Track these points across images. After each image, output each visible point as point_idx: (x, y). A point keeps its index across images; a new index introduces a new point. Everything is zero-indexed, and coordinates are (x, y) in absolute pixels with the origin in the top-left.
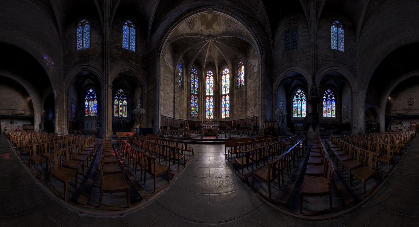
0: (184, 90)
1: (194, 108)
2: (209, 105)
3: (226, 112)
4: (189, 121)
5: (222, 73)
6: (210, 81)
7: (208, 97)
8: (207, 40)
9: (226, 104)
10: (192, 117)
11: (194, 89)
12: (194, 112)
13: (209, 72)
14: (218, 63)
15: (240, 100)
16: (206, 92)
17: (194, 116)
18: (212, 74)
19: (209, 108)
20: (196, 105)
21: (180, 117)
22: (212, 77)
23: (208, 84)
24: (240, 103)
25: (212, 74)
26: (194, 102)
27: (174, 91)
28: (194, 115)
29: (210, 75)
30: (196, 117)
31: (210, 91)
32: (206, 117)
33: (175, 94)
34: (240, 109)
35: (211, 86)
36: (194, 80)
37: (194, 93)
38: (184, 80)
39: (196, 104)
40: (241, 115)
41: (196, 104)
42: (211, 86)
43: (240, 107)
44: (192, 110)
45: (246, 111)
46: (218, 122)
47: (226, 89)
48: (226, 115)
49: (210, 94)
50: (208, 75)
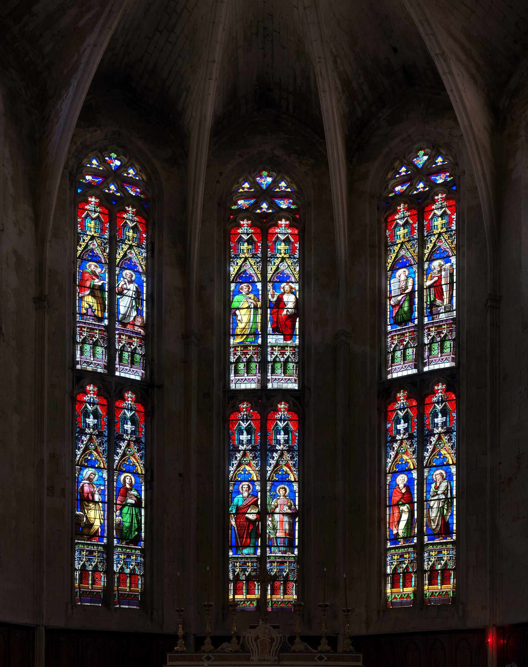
3: (420, 548)
9: (420, 469)
10: (92, 596)
12: (109, 549)
17: (108, 589)
20: (127, 478)
28: (109, 572)
35: (280, 304)
37: (110, 366)
44: (90, 525)
48: (421, 571)
49: (264, 381)
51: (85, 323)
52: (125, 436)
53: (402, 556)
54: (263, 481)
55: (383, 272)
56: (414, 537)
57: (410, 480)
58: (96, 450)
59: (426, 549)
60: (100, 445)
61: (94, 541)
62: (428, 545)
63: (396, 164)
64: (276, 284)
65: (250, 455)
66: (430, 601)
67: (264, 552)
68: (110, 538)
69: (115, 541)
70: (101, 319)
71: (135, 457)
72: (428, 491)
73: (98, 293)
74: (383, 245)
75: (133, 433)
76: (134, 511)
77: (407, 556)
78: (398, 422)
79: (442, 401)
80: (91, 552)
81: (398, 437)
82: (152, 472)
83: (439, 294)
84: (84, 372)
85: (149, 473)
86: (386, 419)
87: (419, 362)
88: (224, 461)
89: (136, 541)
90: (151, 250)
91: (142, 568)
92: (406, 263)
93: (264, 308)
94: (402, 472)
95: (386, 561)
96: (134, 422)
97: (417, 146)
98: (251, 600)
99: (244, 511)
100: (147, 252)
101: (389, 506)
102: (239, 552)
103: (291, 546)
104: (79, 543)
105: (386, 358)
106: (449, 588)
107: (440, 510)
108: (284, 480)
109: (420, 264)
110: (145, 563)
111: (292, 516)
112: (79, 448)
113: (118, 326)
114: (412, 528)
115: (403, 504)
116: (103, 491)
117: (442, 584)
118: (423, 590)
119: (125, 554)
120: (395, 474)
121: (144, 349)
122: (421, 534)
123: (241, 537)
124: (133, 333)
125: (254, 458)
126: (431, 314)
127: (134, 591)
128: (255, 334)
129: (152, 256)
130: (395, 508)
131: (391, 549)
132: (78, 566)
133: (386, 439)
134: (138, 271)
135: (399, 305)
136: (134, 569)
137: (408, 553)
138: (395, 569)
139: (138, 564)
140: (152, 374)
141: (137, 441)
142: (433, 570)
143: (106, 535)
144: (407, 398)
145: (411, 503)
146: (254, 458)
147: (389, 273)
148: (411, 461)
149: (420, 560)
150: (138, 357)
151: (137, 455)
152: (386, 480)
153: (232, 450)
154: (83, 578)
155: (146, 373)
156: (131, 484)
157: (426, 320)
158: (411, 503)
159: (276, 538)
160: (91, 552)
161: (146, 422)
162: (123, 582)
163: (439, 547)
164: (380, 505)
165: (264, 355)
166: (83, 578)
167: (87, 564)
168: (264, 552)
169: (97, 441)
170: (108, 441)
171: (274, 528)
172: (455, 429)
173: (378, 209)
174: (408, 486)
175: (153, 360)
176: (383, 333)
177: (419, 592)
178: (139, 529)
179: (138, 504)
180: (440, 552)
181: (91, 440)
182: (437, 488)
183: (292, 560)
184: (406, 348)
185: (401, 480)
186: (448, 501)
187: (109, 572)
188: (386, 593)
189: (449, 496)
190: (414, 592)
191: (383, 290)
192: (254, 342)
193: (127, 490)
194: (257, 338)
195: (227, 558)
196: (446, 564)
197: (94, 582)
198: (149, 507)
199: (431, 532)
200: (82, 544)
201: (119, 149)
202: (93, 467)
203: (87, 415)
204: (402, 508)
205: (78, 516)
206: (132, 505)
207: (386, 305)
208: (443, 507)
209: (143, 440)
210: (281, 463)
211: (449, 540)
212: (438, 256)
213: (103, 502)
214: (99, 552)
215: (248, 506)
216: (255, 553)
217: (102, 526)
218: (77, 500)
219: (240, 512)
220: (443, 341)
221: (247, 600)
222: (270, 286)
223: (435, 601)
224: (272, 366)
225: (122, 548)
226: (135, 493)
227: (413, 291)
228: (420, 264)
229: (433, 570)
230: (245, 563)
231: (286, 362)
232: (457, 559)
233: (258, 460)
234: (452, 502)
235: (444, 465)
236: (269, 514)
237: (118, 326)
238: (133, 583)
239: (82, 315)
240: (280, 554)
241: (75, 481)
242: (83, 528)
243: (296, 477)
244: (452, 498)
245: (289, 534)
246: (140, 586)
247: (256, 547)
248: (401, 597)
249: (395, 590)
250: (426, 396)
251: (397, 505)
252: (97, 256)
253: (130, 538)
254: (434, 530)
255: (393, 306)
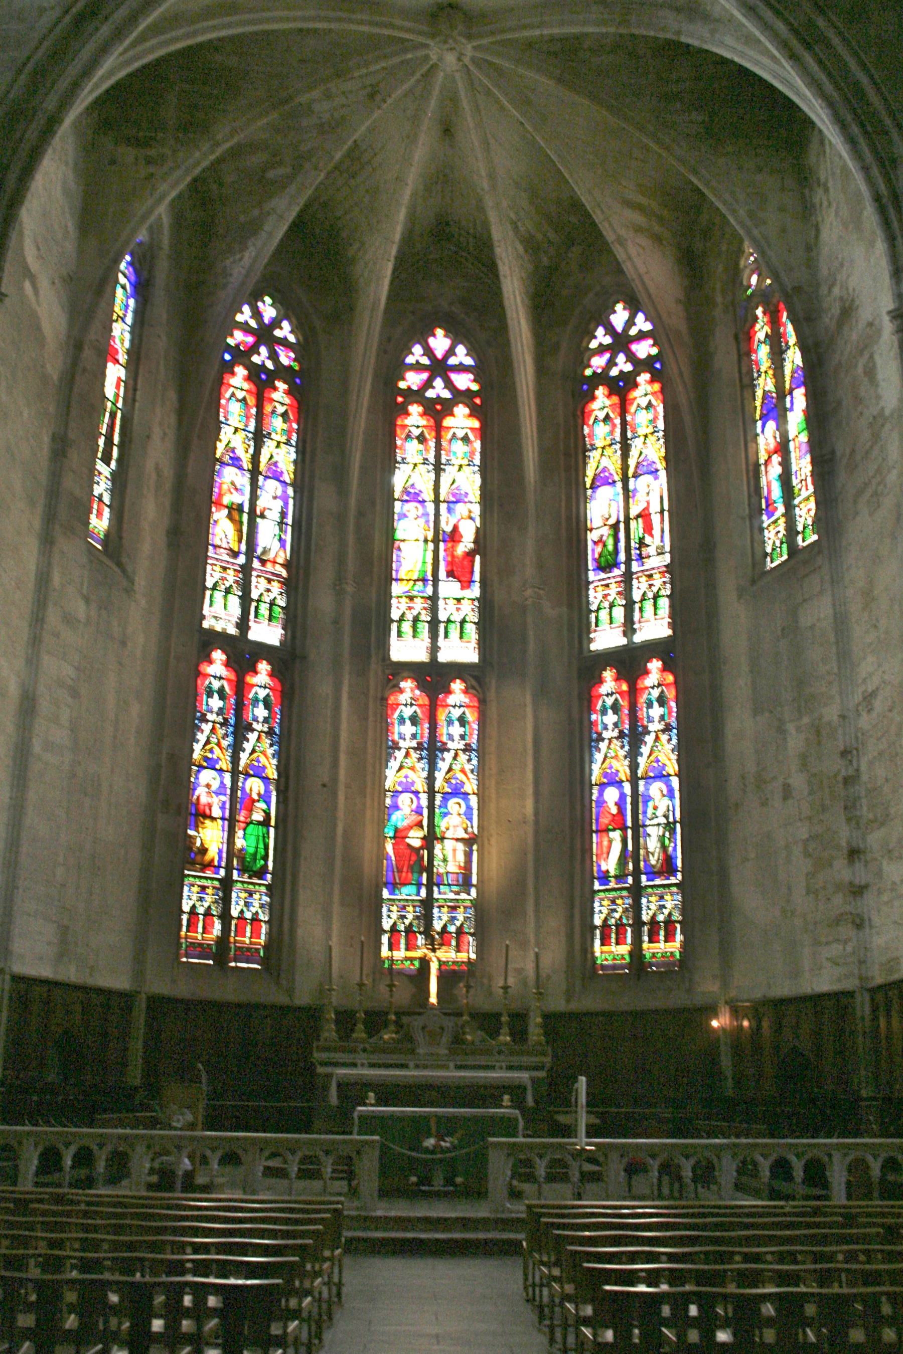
0: (129, 591)
1: (231, 823)
2: (420, 785)
3: (637, 892)
4: (157, 1004)
5: (582, 356)
6: (438, 468)
7: (407, 685)
8: (426, 46)
9: (634, 780)
10: (201, 950)
11: (246, 570)
12: (226, 885)
13: (429, 351)
14: (531, 245)
15: (795, 742)
16: (385, 622)
17: (223, 940)
18: (461, 368)
19: (415, 839)
20: (254, 786)
21: (63, 952)
22: (461, 410)
23: (411, 508)
24: (798, 781)
25: (461, 368)
26: (237, 749)
27: (38, 619)
28: (225, 917)
29: (439, 389)
30: (246, 954)
31: (434, 599)
32: (385, 952)
33: (47, 660)
34: (797, 851)
35: (454, 536)
36: (255, 459)
37: (243, 624)
38: (150, 465)
39: (259, 773)
40: (816, 943)
41: (259, 773)
42: (454, 536)
43: (803, 832)
44: (204, 850)
45: (858, 891)
46: (535, 1033)
47: (628, 577)
48: (638, 924)
49: (434, 649)
50: (413, 380)
51: (217, 559)
52: (255, 725)
53: (613, 902)
54: (431, 793)
55: (581, 491)
56: (627, 875)
57: (623, 796)
58: (219, 744)
59: (643, 893)
60: (223, 738)
61: (209, 874)
62: (646, 887)
63: (592, 326)
64: (452, 505)
65: (414, 755)
66: (651, 965)
67: (430, 892)
68: (229, 869)
69: (235, 873)
70: (235, 554)
71: (265, 755)
72: (645, 812)
73: (236, 515)
74: (580, 451)
75: (266, 720)
76: (261, 830)
77: (619, 901)
78: (604, 712)
79: (659, 685)
80: (203, 888)
81: (606, 735)
82: (287, 778)
83: (648, 529)
84: (211, 632)
85: (283, 780)
86: (591, 709)
87: (629, 627)
88: (381, 763)
89: (261, 873)
90: (301, 449)
91: (267, 911)
92: (607, 478)
93: (436, 541)
94: (611, 783)
95: (593, 908)
96: (267, 705)
97: (614, 298)
98: (411, 959)
99: (403, 834)
100: (296, 452)
101: (597, 832)
102: (397, 892)
103: (466, 884)
104: (189, 876)
105: (588, 619)
106: (674, 947)
107: (661, 839)
108: (457, 792)
109: (625, 480)
110: (271, 905)
111: (469, 842)
112: (197, 741)
113: (256, 564)
114: (627, 863)
115: (614, 830)
116: (224, 803)
117: (666, 941)
118: (641, 949)
119: (246, 891)
120: (602, 786)
121: (285, 599)
122: (637, 873)
123: (400, 871)
124: (273, 574)
125: (420, 759)
126: (640, 557)
127: (256, 944)
128: (424, 580)
129: (303, 461)
130: (604, 834)
131: (599, 891)
132: (186, 907)
133: (591, 736)
134: (284, 482)
135: (600, 541)
136: (257, 913)
137: (622, 897)
138: (606, 920)
139: (262, 906)
140: (294, 637)
141: (270, 733)
142: (653, 922)
143: (223, 864)
144: (617, 679)
145: (624, 829)
146: (420, 759)
147: (589, 492)
148: (622, 768)
149: (636, 908)
150: (277, 610)
151: (270, 752)
152: (591, 794)
153: (392, 748)
154: (191, 925)
155: (286, 635)
156: (259, 794)
157: (635, 566)
158: (624, 829)
159: (447, 873)
160: (203, 888)
161: (282, 705)
162: (240, 932)
163: (661, 890)
164: (583, 829)
165: (434, 610)
166: (191, 925)
167: (198, 904)
168: (430, 892)
169: (221, 732)
170: (234, 733)
171: (445, 860)
172: (674, 724)
173: (573, 396)
174: (620, 804)
175: (295, 617)
176: (583, 583)
177: (636, 952)
178: (265, 858)
179: (266, 823)
180: (662, 898)
181: (213, 730)
182: (655, 808)
183: (468, 904)
184: (612, 606)
185: (611, 795)
186: (670, 827)
187: (225, 917)
188: (593, 953)
189: (671, 819)
190: (631, 953)
191: (582, 519)
192: (422, 592)
193: (254, 801)
194: (425, 585)
195: (380, 901)
196: (670, 914)
197: (205, 930)
198: (281, 827)
199: (649, 870)
200: (194, 877)
201: (276, 294)
202: (214, 769)
203: (210, 694)
204: (611, 834)
205: (190, 836)
206: (259, 823)
207: (586, 540)
208: (664, 835)
209: (277, 730)
210: (454, 767)
211: (673, 880)
212: (645, 469)
213: (223, 819)
214: (214, 888)
215: (410, 828)
216: (418, 894)
217: (220, 852)
218: (191, 814)
219: (400, 835)
220: (656, 597)
221: (407, 959)
222: (443, 507)
223: (657, 965)
224: (446, 628)
225: (243, 882)
226: (264, 806)
227: (618, 522)
228: (625, 480)
229: (653, 922)
230: (404, 908)
231: (463, 622)
232: (684, 909)
233: (424, 764)
234: (675, 829)
235: (662, 776)
236: (437, 839)
237: (256, 564)
238: (256, 933)
239: (215, 547)
240: (452, 896)
241: (190, 788)
242: (196, 854)
243: (475, 788)
244: (675, 822)
245: (465, 868)
246: (263, 937)
247: (419, 885)
248: (614, 959)
249: (605, 948)
250: (638, 677)
251: (607, 830)
252: (238, 459)
253: (255, 869)
254: (653, 866)
255: (595, 543)
